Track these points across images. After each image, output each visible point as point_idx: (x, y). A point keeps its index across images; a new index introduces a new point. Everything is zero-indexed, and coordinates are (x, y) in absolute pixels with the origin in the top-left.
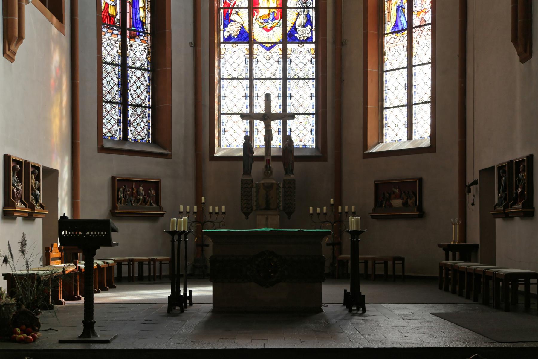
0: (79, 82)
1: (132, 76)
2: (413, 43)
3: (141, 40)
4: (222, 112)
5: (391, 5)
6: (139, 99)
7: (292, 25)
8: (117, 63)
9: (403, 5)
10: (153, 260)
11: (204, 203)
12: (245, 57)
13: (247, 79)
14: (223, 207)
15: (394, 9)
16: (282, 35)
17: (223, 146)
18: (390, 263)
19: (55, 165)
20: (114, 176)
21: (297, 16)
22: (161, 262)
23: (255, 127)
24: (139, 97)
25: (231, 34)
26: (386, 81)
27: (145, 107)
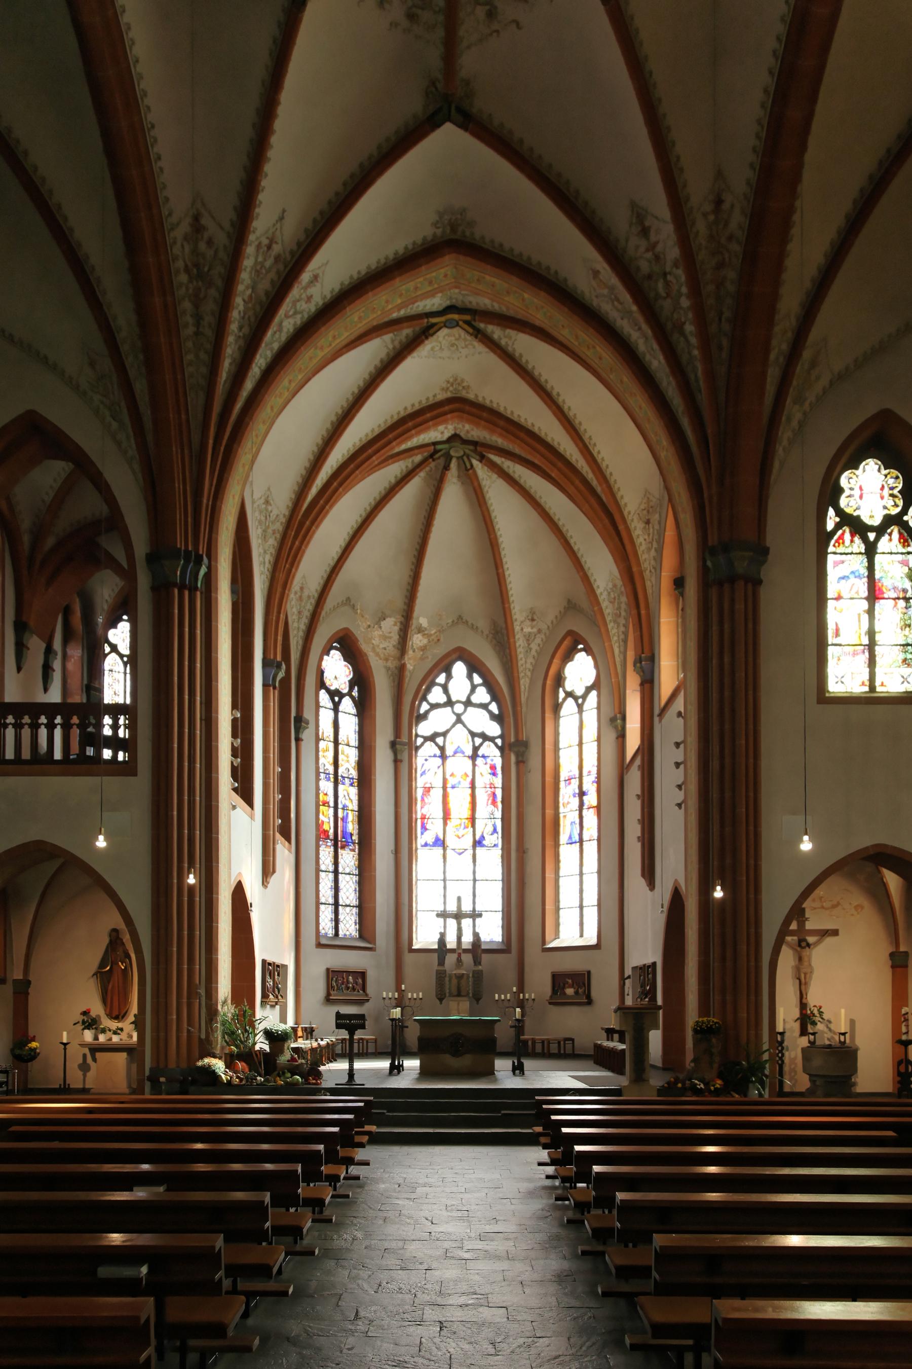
14: (421, 994)
18: (562, 1043)
22: (367, 1041)
23: (395, 315)
27: (353, 906)
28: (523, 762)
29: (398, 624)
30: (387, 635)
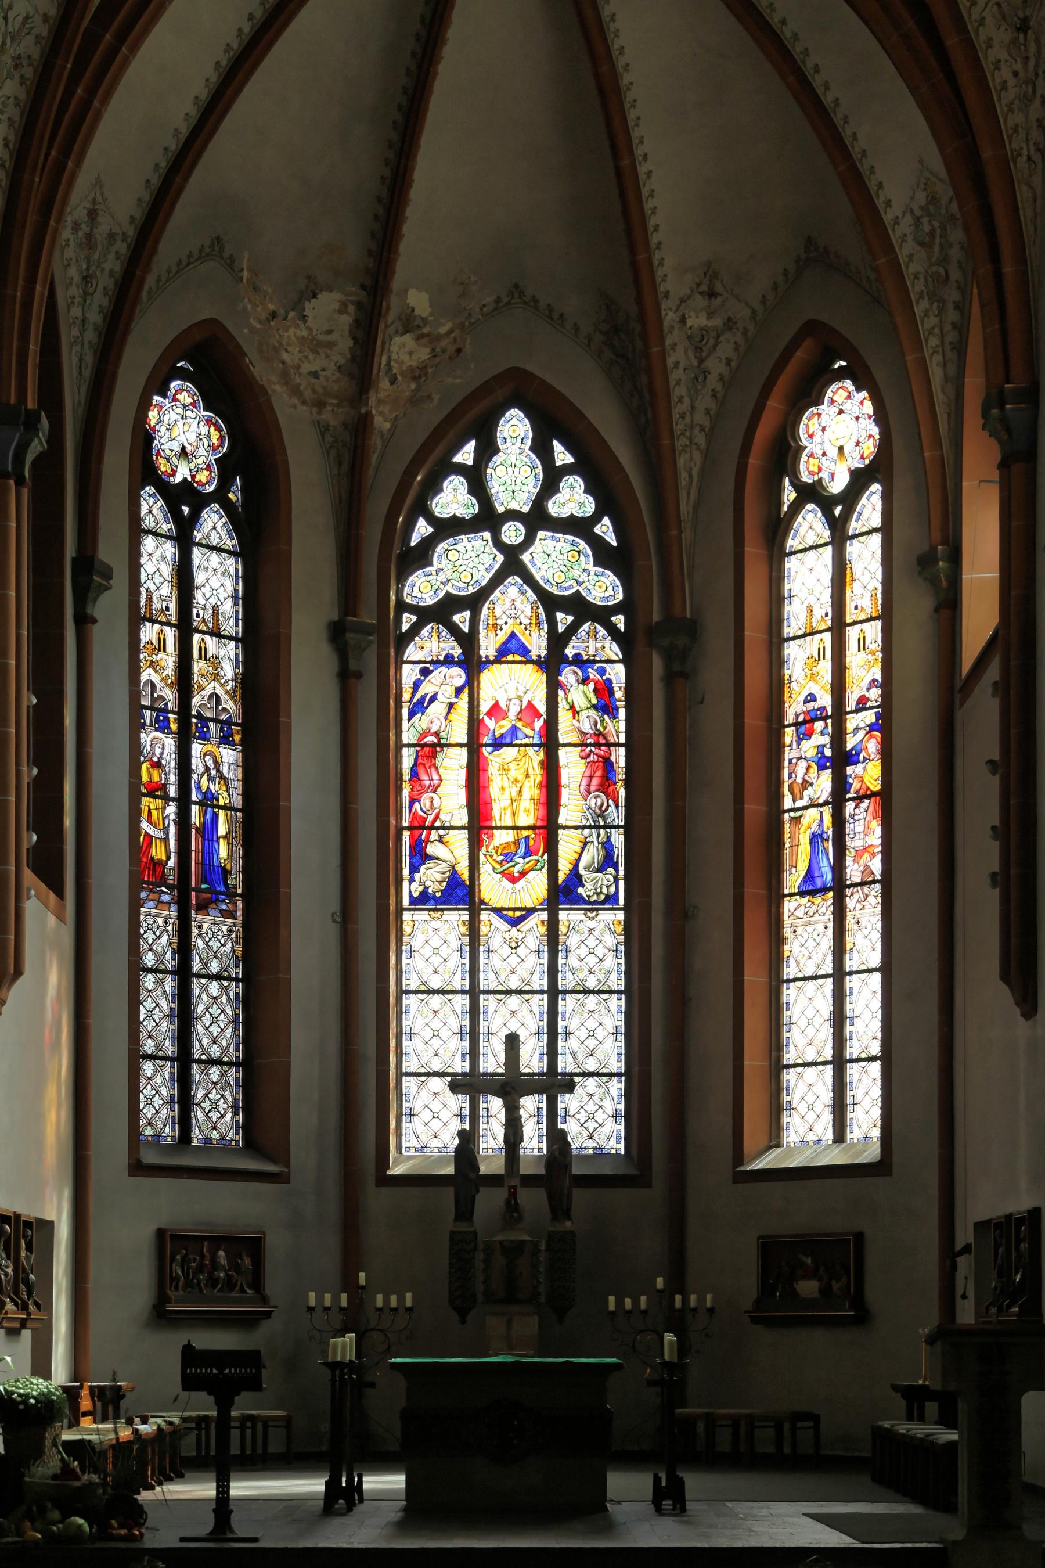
0: (93, 1022)
1: (200, 995)
2: (848, 921)
3: (221, 911)
4: (404, 1071)
5: (799, 829)
6: (215, 1046)
7: (571, 867)
8: (170, 968)
9: (823, 832)
10: (251, 1418)
11: (363, 1288)
12: (460, 942)
13: (463, 992)
14: (409, 1296)
15: (805, 839)
16: (548, 890)
17: (408, 1149)
18: (787, 1426)
19: (49, 1215)
20: (163, 1226)
21: (581, 845)
22: (266, 1422)
23: (482, 1023)
24: (214, 1041)
25: (426, 888)
26: (788, 1004)
27: (230, 1064)
28: (684, 675)
29: (351, 309)
30: (321, 337)
